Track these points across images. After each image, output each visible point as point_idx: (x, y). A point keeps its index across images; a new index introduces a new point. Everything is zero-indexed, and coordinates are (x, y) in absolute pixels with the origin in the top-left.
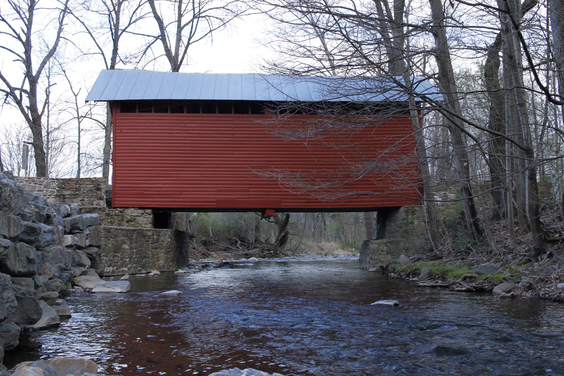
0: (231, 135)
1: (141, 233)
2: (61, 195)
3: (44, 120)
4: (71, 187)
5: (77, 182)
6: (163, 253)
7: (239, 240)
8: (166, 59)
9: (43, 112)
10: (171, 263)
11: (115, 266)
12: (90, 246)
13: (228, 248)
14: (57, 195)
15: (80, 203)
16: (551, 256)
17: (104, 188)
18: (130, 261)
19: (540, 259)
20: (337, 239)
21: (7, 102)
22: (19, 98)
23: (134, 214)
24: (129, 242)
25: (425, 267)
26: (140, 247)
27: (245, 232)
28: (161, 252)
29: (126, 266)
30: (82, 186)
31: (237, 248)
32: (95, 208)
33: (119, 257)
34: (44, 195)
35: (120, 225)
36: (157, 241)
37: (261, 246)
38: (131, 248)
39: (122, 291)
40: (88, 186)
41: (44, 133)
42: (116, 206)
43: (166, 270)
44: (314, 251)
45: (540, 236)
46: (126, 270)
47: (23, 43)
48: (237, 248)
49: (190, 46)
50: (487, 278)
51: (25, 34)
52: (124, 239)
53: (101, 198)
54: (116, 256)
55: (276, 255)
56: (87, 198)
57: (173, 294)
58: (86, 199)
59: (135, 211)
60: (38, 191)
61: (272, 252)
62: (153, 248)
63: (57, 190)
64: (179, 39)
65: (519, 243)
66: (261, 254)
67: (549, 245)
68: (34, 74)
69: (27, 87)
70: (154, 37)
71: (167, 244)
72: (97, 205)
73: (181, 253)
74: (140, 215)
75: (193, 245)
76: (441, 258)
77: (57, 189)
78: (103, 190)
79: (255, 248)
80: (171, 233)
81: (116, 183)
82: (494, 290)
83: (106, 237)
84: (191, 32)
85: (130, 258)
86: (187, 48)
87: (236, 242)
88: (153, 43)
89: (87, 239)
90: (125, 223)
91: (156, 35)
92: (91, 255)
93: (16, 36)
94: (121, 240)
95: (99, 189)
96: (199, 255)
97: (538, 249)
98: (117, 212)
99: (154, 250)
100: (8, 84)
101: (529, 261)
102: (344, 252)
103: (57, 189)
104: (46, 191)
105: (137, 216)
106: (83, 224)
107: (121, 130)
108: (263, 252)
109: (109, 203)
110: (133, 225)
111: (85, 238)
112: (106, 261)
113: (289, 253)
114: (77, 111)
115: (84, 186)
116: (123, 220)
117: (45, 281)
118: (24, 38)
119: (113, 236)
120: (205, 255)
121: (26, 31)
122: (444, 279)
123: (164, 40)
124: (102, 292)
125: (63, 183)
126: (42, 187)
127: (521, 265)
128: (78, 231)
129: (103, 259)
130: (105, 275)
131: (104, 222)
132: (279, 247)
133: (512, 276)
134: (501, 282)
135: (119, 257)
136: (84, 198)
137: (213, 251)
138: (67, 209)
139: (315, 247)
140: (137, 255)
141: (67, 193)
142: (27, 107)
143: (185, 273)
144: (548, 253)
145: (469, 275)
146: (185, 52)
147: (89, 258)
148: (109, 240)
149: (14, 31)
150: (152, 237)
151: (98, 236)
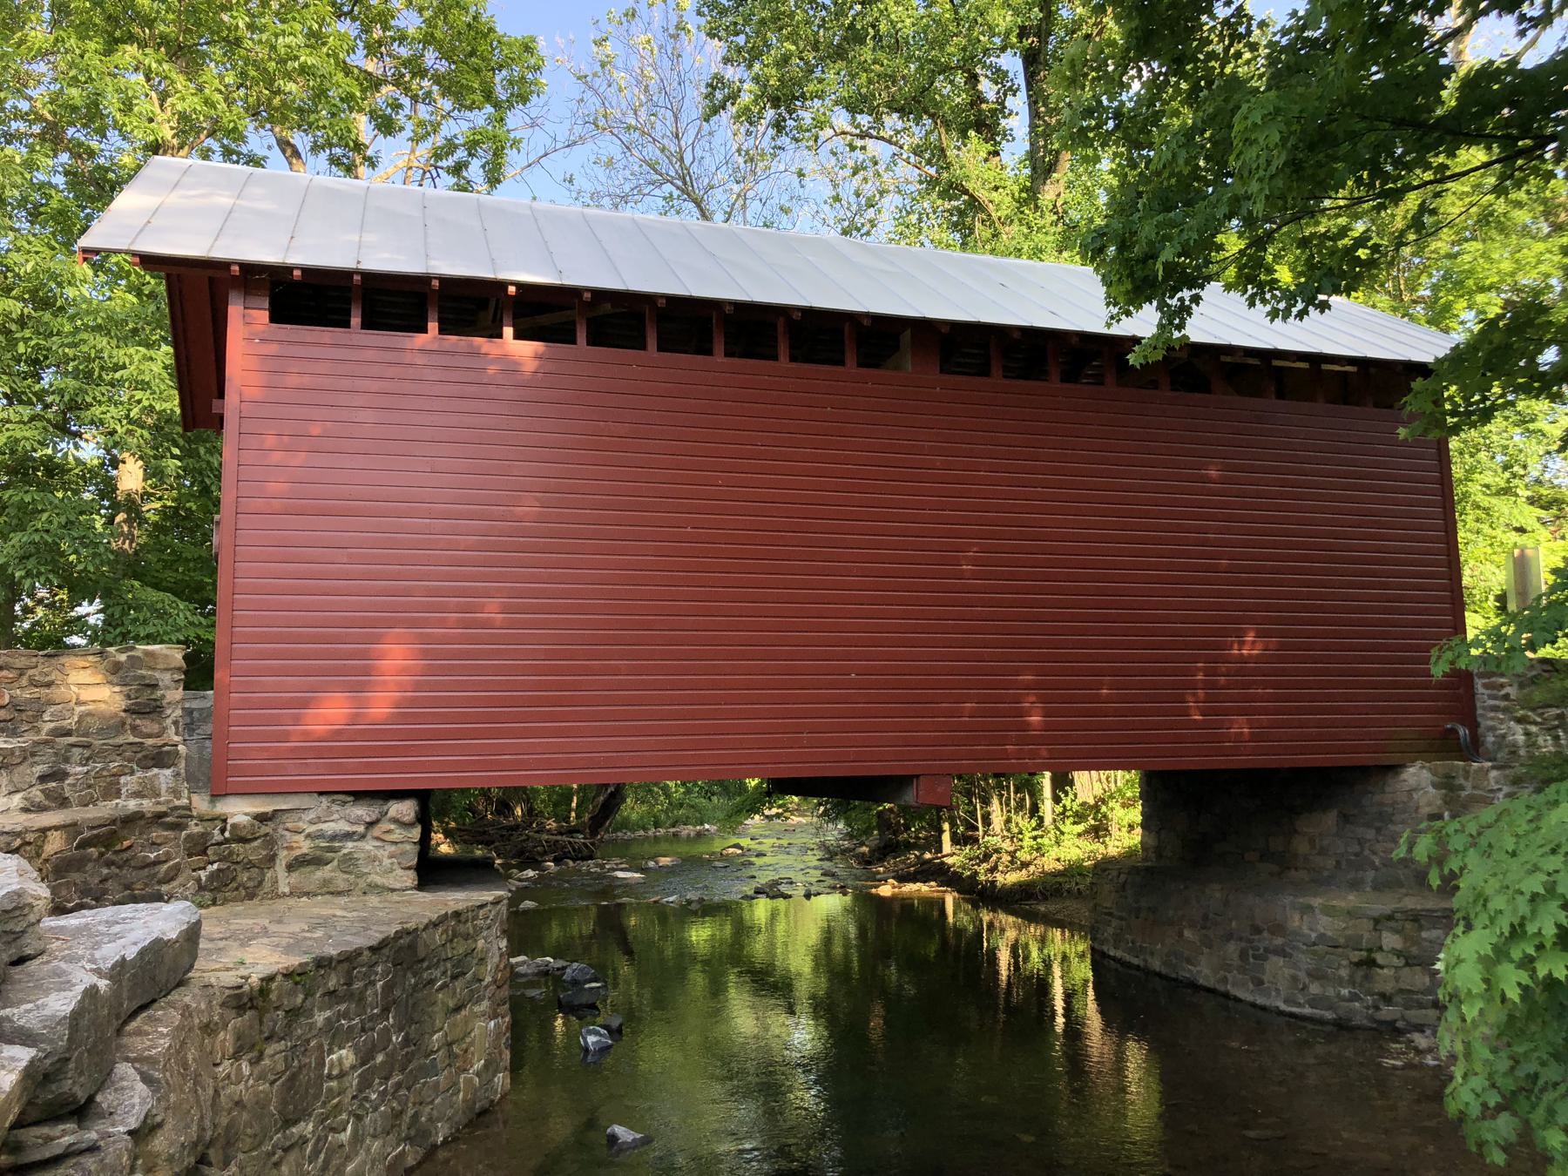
23: (330, 827)
56: (85, 761)
72: (137, 794)
74: (361, 829)
105: (348, 836)
136: (67, 760)
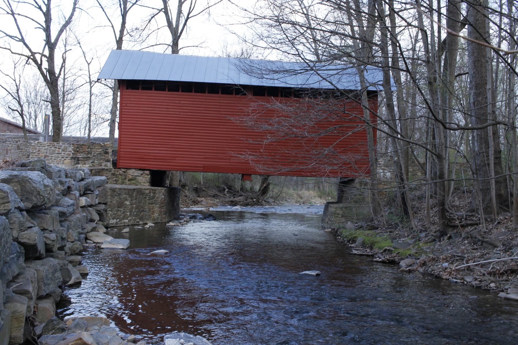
0: (217, 112)
1: (140, 192)
2: (75, 157)
3: (60, 82)
4: (84, 151)
5: (89, 146)
6: (158, 207)
7: (227, 188)
8: (167, 29)
10: (164, 216)
12: (99, 203)
13: (216, 194)
14: (72, 158)
15: (91, 165)
16: (450, 238)
17: (110, 152)
18: (130, 215)
19: (442, 240)
20: (316, 188)
21: (28, 63)
22: (39, 63)
23: (135, 174)
24: (130, 199)
25: (362, 236)
26: (139, 203)
27: (232, 181)
28: (156, 207)
29: (127, 219)
30: (93, 150)
31: (224, 195)
32: (103, 169)
33: (121, 211)
34: (62, 157)
35: (123, 183)
36: (153, 197)
37: (245, 195)
38: (131, 204)
39: (124, 247)
40: (98, 150)
41: (60, 93)
42: (120, 167)
43: (160, 221)
44: (294, 199)
45: (444, 222)
46: (126, 222)
47: (44, 13)
48: (224, 195)
49: (189, 20)
50: (399, 253)
51: (46, 5)
52: (126, 197)
53: (108, 161)
54: (119, 211)
55: (258, 203)
56: (97, 160)
57: (162, 252)
58: (96, 162)
60: (57, 154)
61: (255, 200)
63: (73, 153)
64: (180, 12)
65: (433, 224)
66: (245, 202)
67: (450, 229)
69: (47, 53)
70: (158, 10)
71: (161, 200)
73: (173, 206)
74: (140, 175)
75: (185, 193)
76: (377, 228)
77: (73, 152)
79: (240, 196)
80: (165, 191)
81: (121, 148)
82: (400, 264)
83: (112, 196)
84: (190, 8)
85: (131, 212)
87: (224, 190)
88: (157, 14)
89: (96, 198)
90: (127, 181)
92: (99, 211)
93: (38, 7)
94: (124, 198)
95: (107, 153)
96: (190, 202)
97: (442, 232)
98: (121, 172)
99: (150, 205)
101: (434, 240)
102: (321, 201)
103: (73, 152)
104: (64, 154)
105: (138, 176)
106: (94, 186)
107: (126, 104)
108: (247, 200)
109: (115, 164)
110: (134, 183)
111: (95, 198)
112: (111, 215)
113: (271, 200)
114: (90, 78)
115: (95, 150)
116: (126, 179)
117: (70, 247)
118: (44, 9)
119: (117, 195)
120: (195, 202)
121: (46, 3)
122: (371, 248)
123: (166, 13)
124: (108, 248)
125: (78, 148)
126: (61, 150)
127: (427, 243)
128: (90, 192)
129: (109, 213)
130: (110, 226)
132: (261, 196)
133: (416, 253)
134: (407, 257)
135: (121, 211)
136: (95, 160)
137: (203, 197)
138: (82, 175)
139: (295, 195)
140: (136, 209)
142: (46, 69)
143: (174, 225)
144: (448, 235)
145: (388, 248)
146: (185, 24)
148: (114, 197)
149: (36, 3)
150: (149, 195)
151: (105, 195)
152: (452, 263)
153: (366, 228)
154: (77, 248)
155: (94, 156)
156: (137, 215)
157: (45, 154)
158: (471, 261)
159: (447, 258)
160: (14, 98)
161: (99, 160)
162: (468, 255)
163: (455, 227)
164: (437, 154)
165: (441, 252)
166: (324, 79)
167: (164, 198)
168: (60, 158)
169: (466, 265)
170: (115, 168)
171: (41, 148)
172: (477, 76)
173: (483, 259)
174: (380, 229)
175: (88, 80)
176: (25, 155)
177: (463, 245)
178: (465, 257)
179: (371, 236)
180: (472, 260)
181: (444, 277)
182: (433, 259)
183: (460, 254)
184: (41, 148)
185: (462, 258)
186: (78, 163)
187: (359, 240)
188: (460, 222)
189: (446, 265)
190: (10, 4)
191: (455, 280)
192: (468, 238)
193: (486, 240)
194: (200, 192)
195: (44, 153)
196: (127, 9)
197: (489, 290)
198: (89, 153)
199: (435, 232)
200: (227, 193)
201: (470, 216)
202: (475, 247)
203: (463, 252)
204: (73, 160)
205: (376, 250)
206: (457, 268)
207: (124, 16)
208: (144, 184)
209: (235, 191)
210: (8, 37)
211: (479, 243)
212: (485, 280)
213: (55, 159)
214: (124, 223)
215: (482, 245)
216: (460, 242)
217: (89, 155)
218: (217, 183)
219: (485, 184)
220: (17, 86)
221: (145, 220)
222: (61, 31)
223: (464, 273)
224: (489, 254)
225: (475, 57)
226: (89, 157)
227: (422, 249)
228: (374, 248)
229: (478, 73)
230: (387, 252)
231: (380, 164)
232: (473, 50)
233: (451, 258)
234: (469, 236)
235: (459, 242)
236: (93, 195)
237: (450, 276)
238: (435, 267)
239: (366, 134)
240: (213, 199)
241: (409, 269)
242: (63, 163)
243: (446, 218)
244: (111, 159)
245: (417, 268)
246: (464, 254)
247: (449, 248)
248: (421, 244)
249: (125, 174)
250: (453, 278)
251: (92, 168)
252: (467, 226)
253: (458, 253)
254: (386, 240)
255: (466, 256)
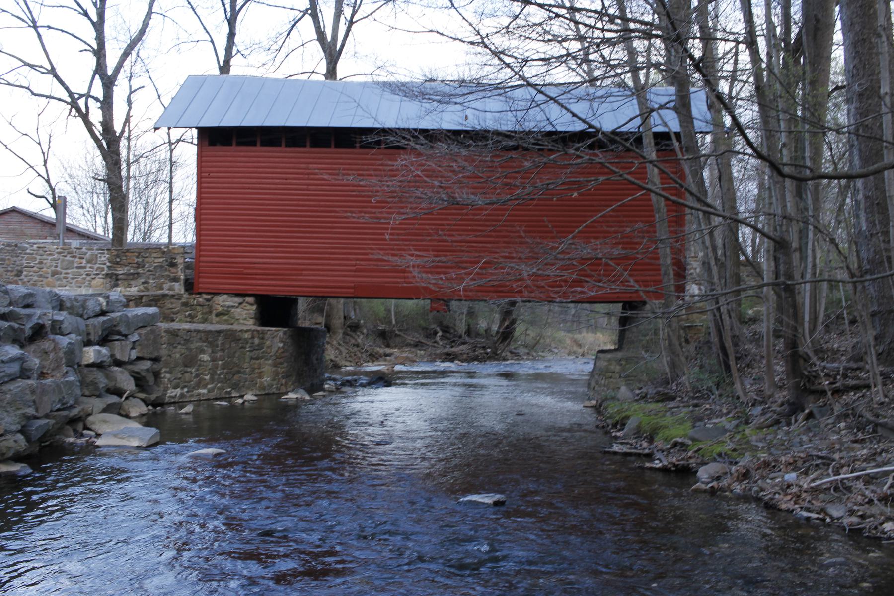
1: (232, 336)
4: (130, 261)
5: (139, 253)
8: (317, 46)
9: (123, 132)
10: (283, 381)
11: (185, 387)
12: (139, 358)
14: (107, 275)
16: (810, 416)
18: (212, 379)
19: (793, 421)
23: (227, 304)
24: (210, 350)
26: (229, 357)
29: (205, 387)
30: (146, 260)
31: (435, 342)
32: (164, 295)
33: (192, 373)
35: (205, 321)
36: (260, 346)
38: (213, 360)
39: (141, 444)
40: (156, 260)
42: (200, 290)
43: (274, 391)
45: (798, 383)
46: (204, 394)
48: (435, 342)
49: (354, 26)
50: (699, 450)
53: (176, 279)
54: (187, 372)
55: (495, 356)
56: (154, 279)
58: (152, 281)
59: (230, 299)
60: (77, 268)
61: (489, 350)
62: (252, 358)
63: (108, 267)
65: (781, 388)
66: (471, 354)
67: (811, 398)
68: (110, 73)
69: (98, 90)
72: (169, 289)
76: (673, 399)
77: (108, 264)
78: (181, 267)
79: (464, 343)
80: (285, 333)
82: (699, 474)
86: (348, 30)
87: (436, 333)
89: (133, 348)
90: (214, 317)
91: (303, 9)
92: (138, 373)
95: (173, 265)
97: (793, 404)
98: (200, 300)
99: (253, 361)
100: (67, 89)
101: (777, 422)
103: (108, 264)
105: (233, 307)
108: (474, 351)
109: (189, 286)
110: (226, 320)
112: (169, 380)
116: (210, 312)
118: (95, 18)
122: (651, 440)
124: (109, 446)
125: (117, 256)
126: (84, 261)
128: (117, 337)
129: (164, 377)
131: (179, 316)
133: (734, 450)
134: (714, 460)
135: (192, 373)
137: (395, 347)
138: (100, 305)
139: (568, 341)
140: (223, 369)
141: (120, 272)
144: (807, 411)
145: (680, 440)
147: (132, 376)
148: (176, 347)
149: (79, 5)
150: (250, 341)
152: (806, 473)
153: (653, 398)
154: (9, 448)
155: (149, 271)
156: (225, 380)
157: (53, 268)
158: (845, 469)
159: (795, 462)
160: (40, 175)
161: (158, 278)
162: (842, 455)
163: (823, 393)
164: (778, 239)
165: (787, 449)
166: (551, 99)
167: (283, 347)
168: (84, 276)
169: (833, 478)
170: (190, 294)
171: (45, 257)
172: (861, 73)
173: (873, 464)
174: (679, 399)
175: (167, 141)
176: (12, 271)
177: (835, 432)
178: (834, 460)
179: (656, 415)
180: (849, 466)
181: (784, 506)
182: (766, 464)
183: (824, 454)
184: (45, 257)
185: (827, 462)
186: (117, 285)
187: (631, 424)
188: (831, 384)
189: (791, 477)
190: (28, 9)
191: (805, 514)
192: (846, 416)
193: (881, 421)
194: (391, 338)
195: (51, 266)
196: (238, 8)
197: (880, 539)
198: (139, 265)
199: (782, 405)
200: (441, 339)
201: (853, 369)
202: (860, 435)
203: (832, 449)
204: (109, 280)
205: (659, 443)
206: (813, 485)
207: (232, 22)
208: (245, 322)
209: (455, 336)
210: (28, 67)
211: (870, 428)
212: (872, 515)
213: (73, 279)
214: (199, 395)
215: (875, 431)
216: (830, 426)
217: (140, 270)
218: (422, 323)
219: (885, 300)
220: (44, 153)
221: (244, 389)
222: (126, 54)
223: (828, 497)
224: (887, 451)
225: (857, 33)
226: (138, 273)
227: (748, 442)
228: (656, 439)
229: (864, 67)
230: (678, 448)
231: (691, 274)
232: (851, 19)
233: (804, 462)
234: (850, 412)
235: (828, 424)
236: (123, 343)
237: (795, 503)
238: (768, 481)
239: (652, 211)
240: (413, 349)
241: (712, 487)
242: (90, 286)
243: (802, 376)
244: (182, 277)
245: (730, 485)
246: (834, 453)
247: (805, 438)
248: (747, 431)
249: (210, 303)
250: (801, 508)
251: (142, 294)
252: (848, 392)
253: (820, 450)
254: (681, 422)
255: (837, 456)
